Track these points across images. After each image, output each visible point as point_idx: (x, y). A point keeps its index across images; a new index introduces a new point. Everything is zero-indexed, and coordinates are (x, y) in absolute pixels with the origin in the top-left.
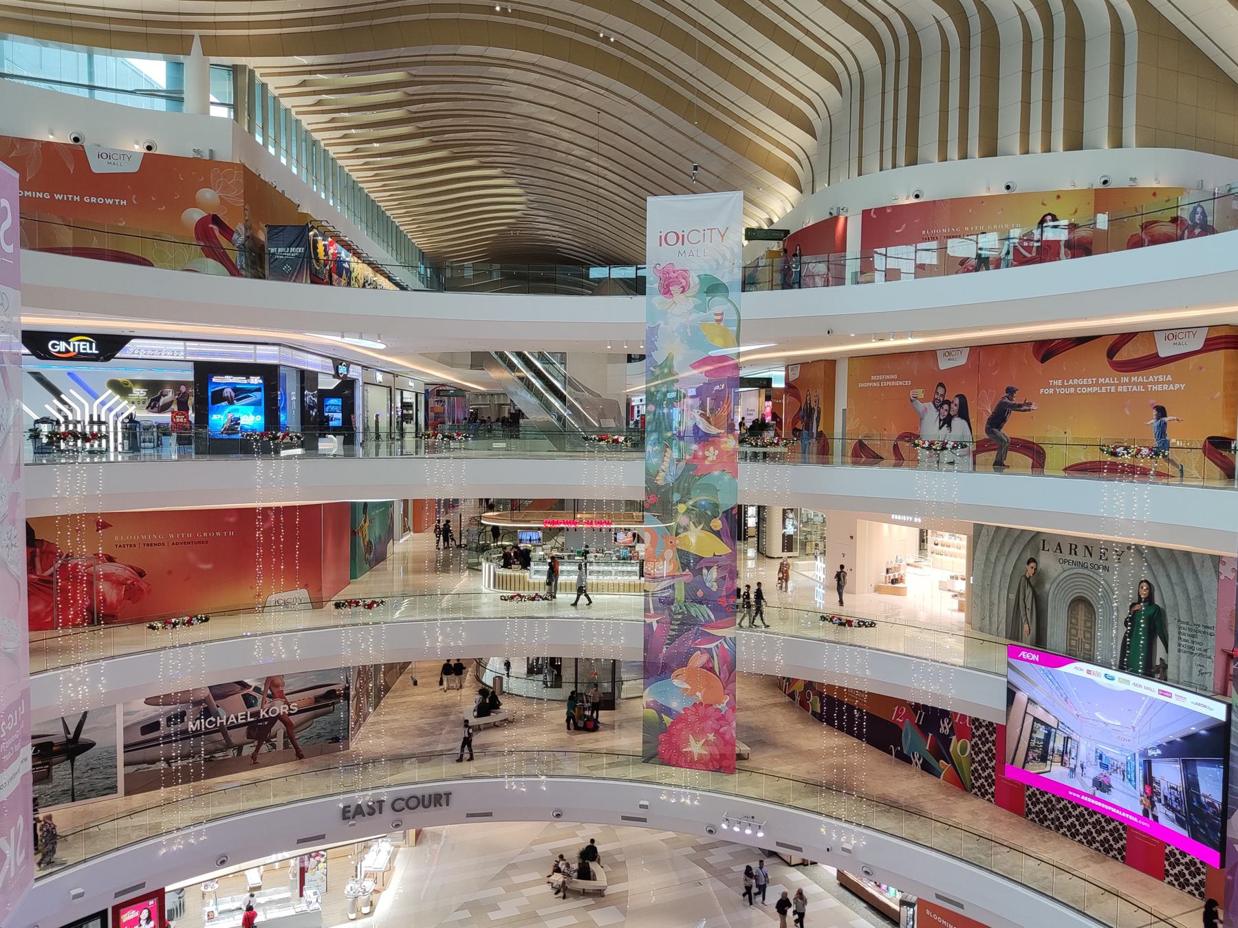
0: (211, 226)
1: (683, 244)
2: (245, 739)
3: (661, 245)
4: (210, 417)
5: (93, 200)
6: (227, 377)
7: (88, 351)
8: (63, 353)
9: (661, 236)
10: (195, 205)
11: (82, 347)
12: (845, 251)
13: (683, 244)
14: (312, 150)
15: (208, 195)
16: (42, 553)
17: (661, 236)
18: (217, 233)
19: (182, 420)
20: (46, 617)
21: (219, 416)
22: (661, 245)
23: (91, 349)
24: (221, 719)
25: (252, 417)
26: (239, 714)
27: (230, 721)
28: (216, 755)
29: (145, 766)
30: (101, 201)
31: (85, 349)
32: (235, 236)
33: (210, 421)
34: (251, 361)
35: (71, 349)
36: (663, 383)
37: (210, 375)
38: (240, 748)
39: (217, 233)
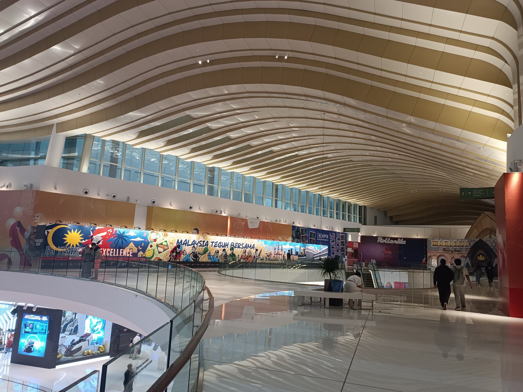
0: (17, 228)
4: (20, 339)
21: (24, 340)
32: (26, 233)
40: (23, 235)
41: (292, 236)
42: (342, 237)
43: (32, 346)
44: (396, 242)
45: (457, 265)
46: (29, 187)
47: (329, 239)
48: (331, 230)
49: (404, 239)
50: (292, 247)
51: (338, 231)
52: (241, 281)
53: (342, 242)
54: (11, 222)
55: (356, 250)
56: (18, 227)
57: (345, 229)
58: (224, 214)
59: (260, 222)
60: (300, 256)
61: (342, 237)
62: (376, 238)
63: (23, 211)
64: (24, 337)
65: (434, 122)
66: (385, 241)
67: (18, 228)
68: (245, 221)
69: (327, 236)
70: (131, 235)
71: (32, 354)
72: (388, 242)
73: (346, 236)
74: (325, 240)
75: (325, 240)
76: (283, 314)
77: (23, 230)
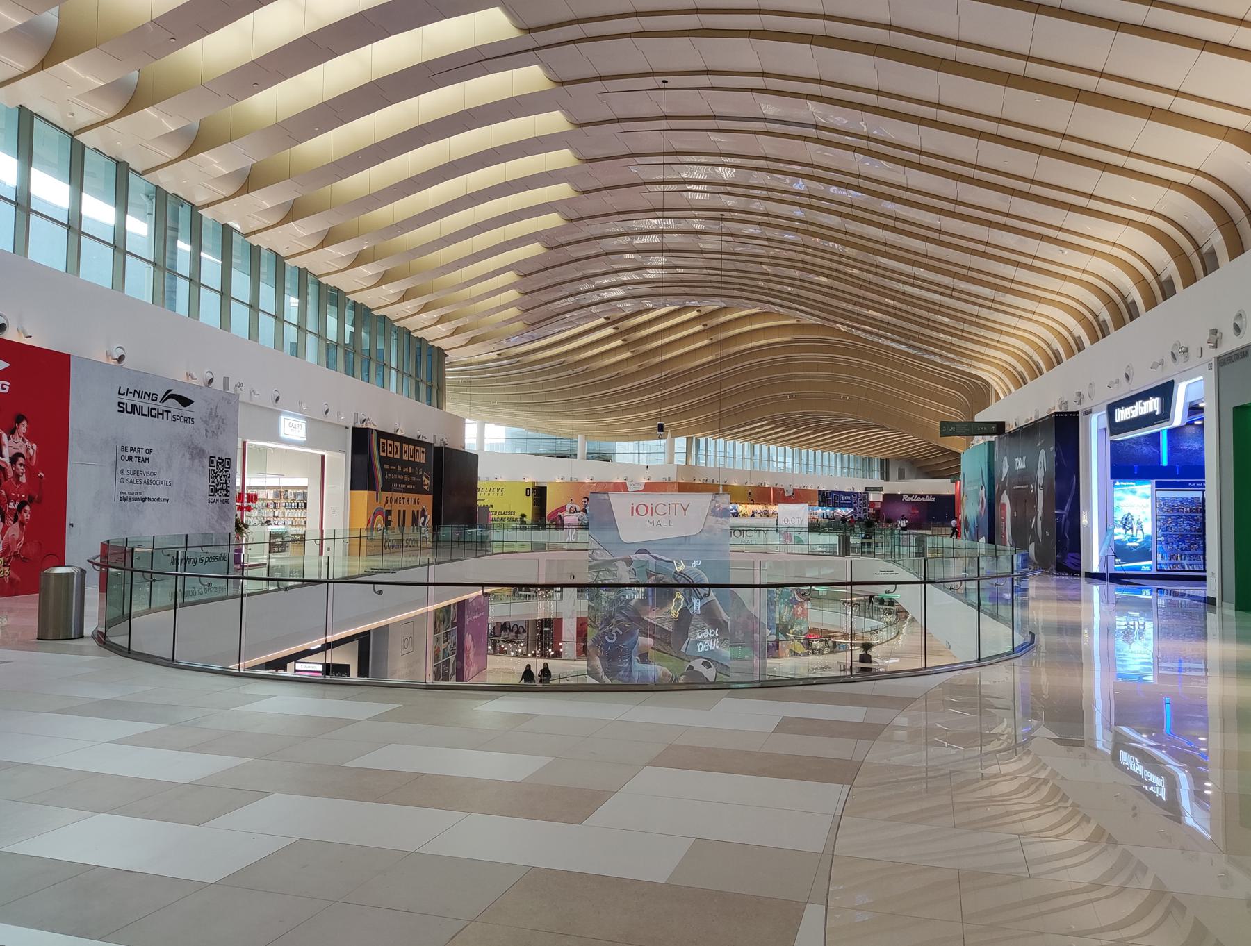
1: (652, 515)
3: (632, 515)
9: (633, 508)
13: (652, 515)
17: (633, 508)
22: (632, 515)
41: (819, 501)
42: (864, 497)
44: (923, 499)
47: (851, 500)
48: (852, 490)
49: (933, 496)
50: (824, 511)
51: (859, 491)
53: (864, 503)
55: (878, 511)
57: (866, 489)
58: (767, 486)
59: (384, 491)
60: (830, 519)
61: (864, 497)
62: (902, 495)
65: (1036, 241)
66: (911, 499)
68: (782, 489)
69: (848, 498)
70: (493, 425)
72: (914, 500)
73: (868, 494)
74: (848, 502)
75: (848, 502)
76: (746, 507)
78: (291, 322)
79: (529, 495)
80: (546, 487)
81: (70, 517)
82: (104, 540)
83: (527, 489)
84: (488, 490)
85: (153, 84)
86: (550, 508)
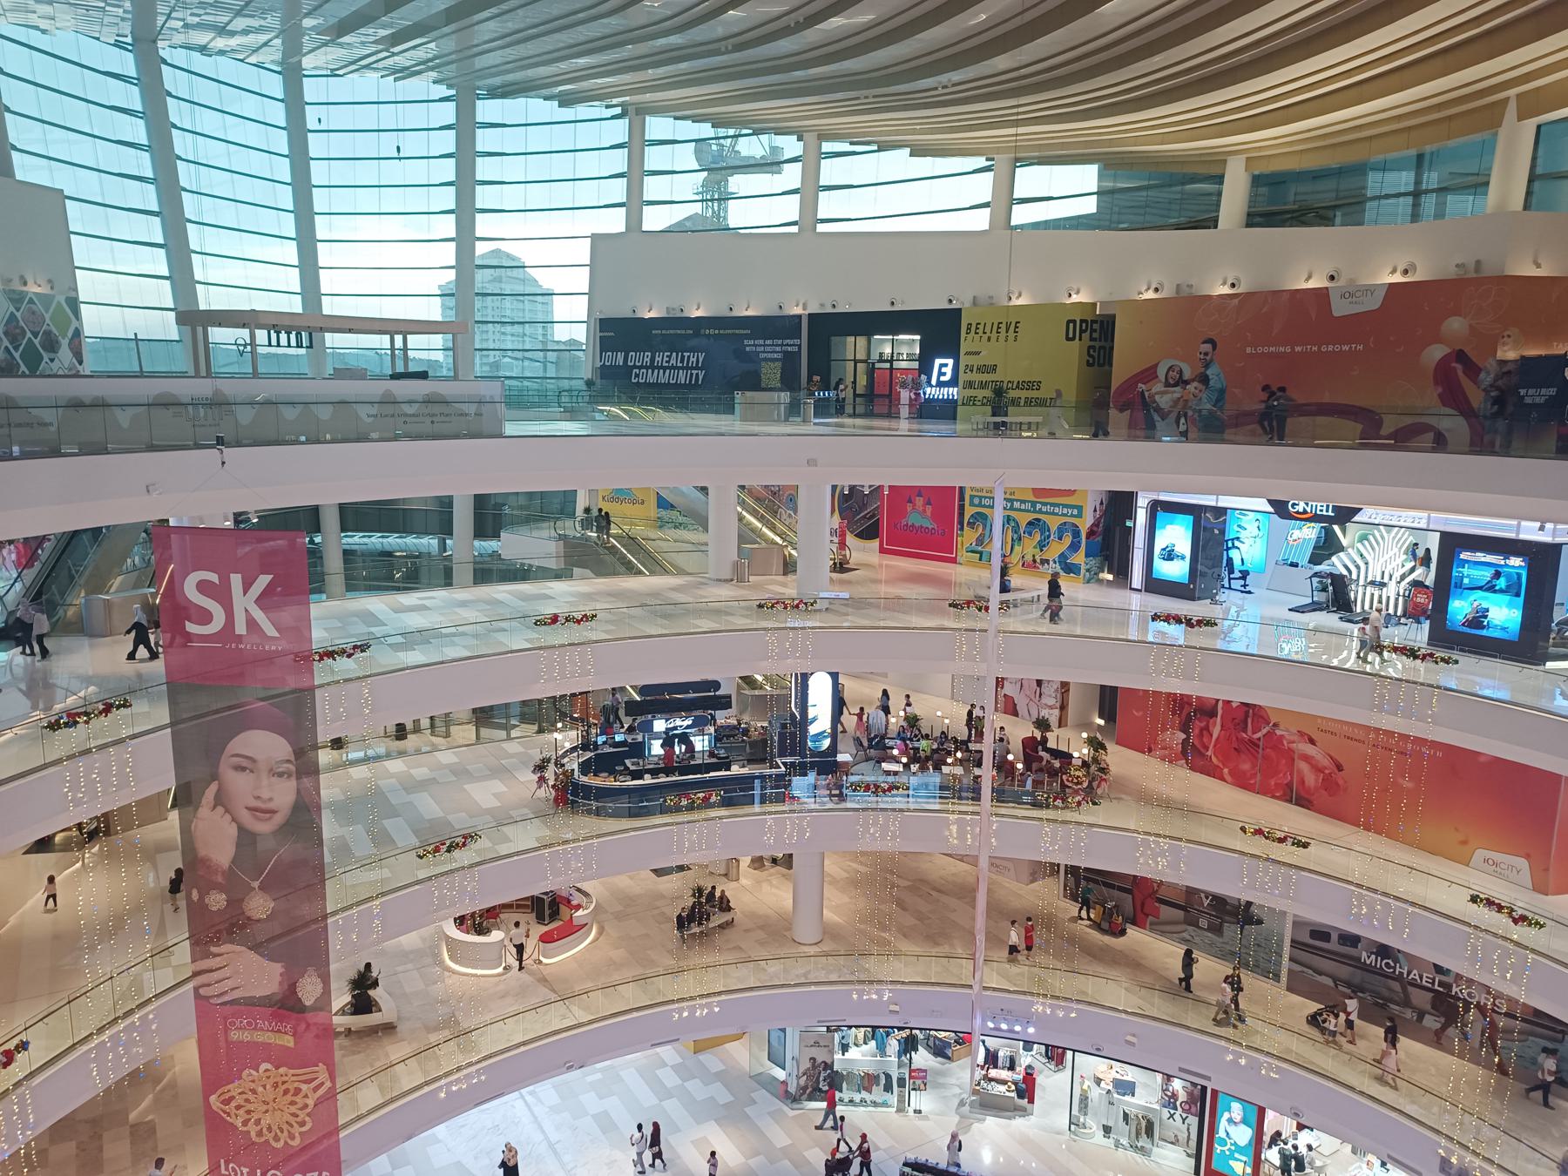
0: (1454, 365)
2: (1428, 1007)
4: (1450, 601)
5: (1330, 348)
6: (1478, 554)
7: (1324, 513)
8: (1300, 513)
10: (1438, 340)
11: (1319, 508)
12: (1560, 776)
14: (725, 425)
15: (1456, 325)
16: (1254, 714)
18: (1460, 373)
19: (1422, 601)
20: (1250, 779)
21: (1463, 603)
23: (1327, 511)
24: (1400, 967)
25: (1505, 611)
26: (1425, 975)
27: (1411, 976)
28: (1392, 1006)
29: (1310, 972)
30: (1337, 348)
31: (1321, 511)
32: (1482, 375)
33: (1450, 608)
34: (1512, 535)
35: (1309, 510)
36: (1380, 900)
37: (1457, 549)
38: (1421, 1015)
39: (1460, 373)
40: (1475, 380)
43: (1486, 617)
45: (1360, 1017)
46: (1472, 267)
52: (1175, 632)
54: (1437, 352)
56: (1457, 362)
63: (1470, 326)
64: (1461, 597)
67: (1459, 367)
71: (1484, 632)
77: (1473, 370)
78: (196, 101)
79: (1073, 339)
80: (1114, 316)
81: (248, 308)
82: (398, 1029)
83: (1069, 322)
84: (988, 330)
85: (124, 323)
86: (1120, 372)
